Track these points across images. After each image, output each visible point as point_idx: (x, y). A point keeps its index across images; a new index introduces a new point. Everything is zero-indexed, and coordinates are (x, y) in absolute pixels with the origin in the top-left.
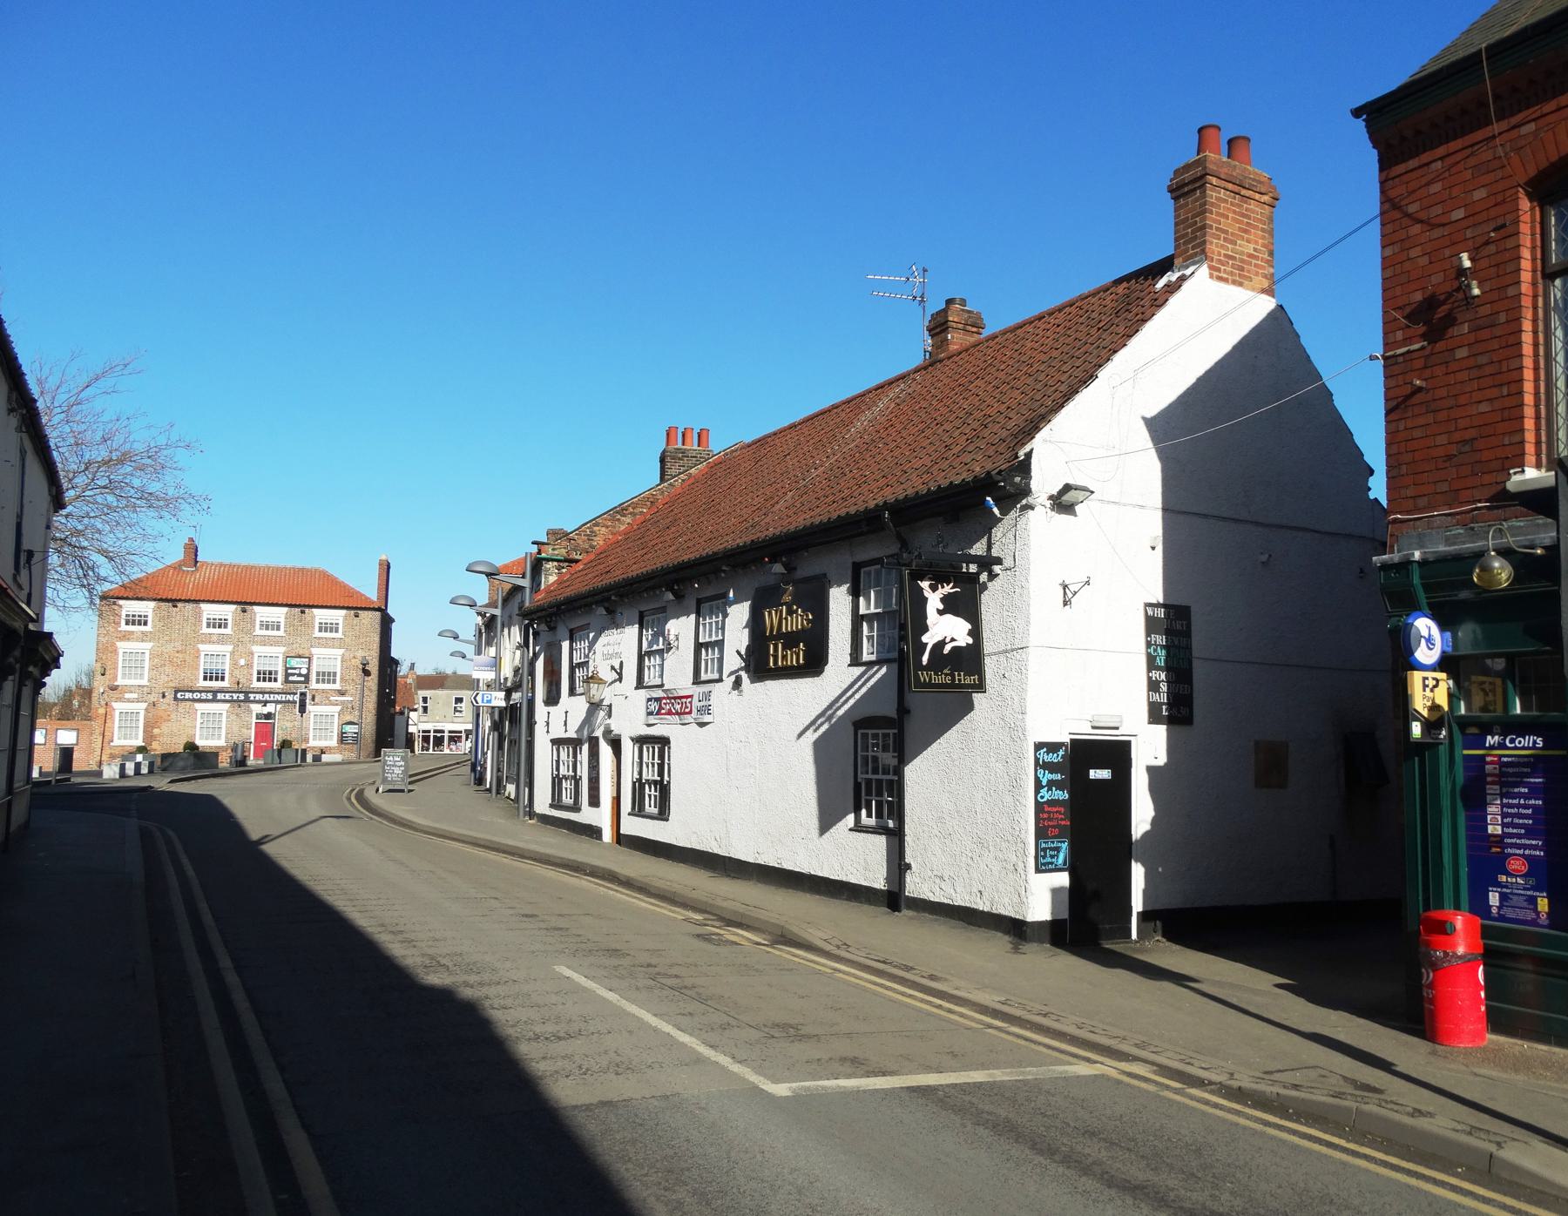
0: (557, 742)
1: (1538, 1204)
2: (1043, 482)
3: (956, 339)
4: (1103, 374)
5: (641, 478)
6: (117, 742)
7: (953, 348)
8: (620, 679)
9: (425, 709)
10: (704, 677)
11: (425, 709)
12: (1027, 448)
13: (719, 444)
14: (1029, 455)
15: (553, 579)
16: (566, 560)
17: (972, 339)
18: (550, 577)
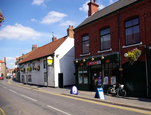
1: (68, 112)
2: (55, 54)
5: (30, 50)
9: (10, 73)
11: (10, 73)
13: (38, 47)
15: (21, 61)
17: (56, 40)
18: (21, 60)
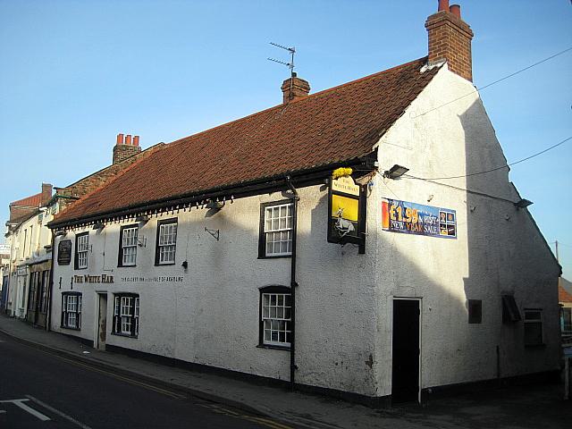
2: (384, 163)
4: (409, 110)
10: (161, 263)
12: (376, 146)
13: (144, 145)
14: (377, 149)
16: (71, 198)
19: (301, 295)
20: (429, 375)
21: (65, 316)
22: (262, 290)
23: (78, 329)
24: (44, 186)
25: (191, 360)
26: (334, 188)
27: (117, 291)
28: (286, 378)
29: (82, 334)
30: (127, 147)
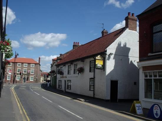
0: (59, 81)
3: (105, 34)
6: (7, 80)
7: (104, 35)
8: (71, 81)
14: (106, 50)
17: (107, 34)
19: (96, 79)
20: (119, 96)
21: (59, 85)
22: (90, 79)
23: (61, 88)
24: (60, 54)
25: (79, 93)
26: (96, 58)
27: (68, 79)
28: (93, 96)
29: (62, 90)
30: (76, 45)
